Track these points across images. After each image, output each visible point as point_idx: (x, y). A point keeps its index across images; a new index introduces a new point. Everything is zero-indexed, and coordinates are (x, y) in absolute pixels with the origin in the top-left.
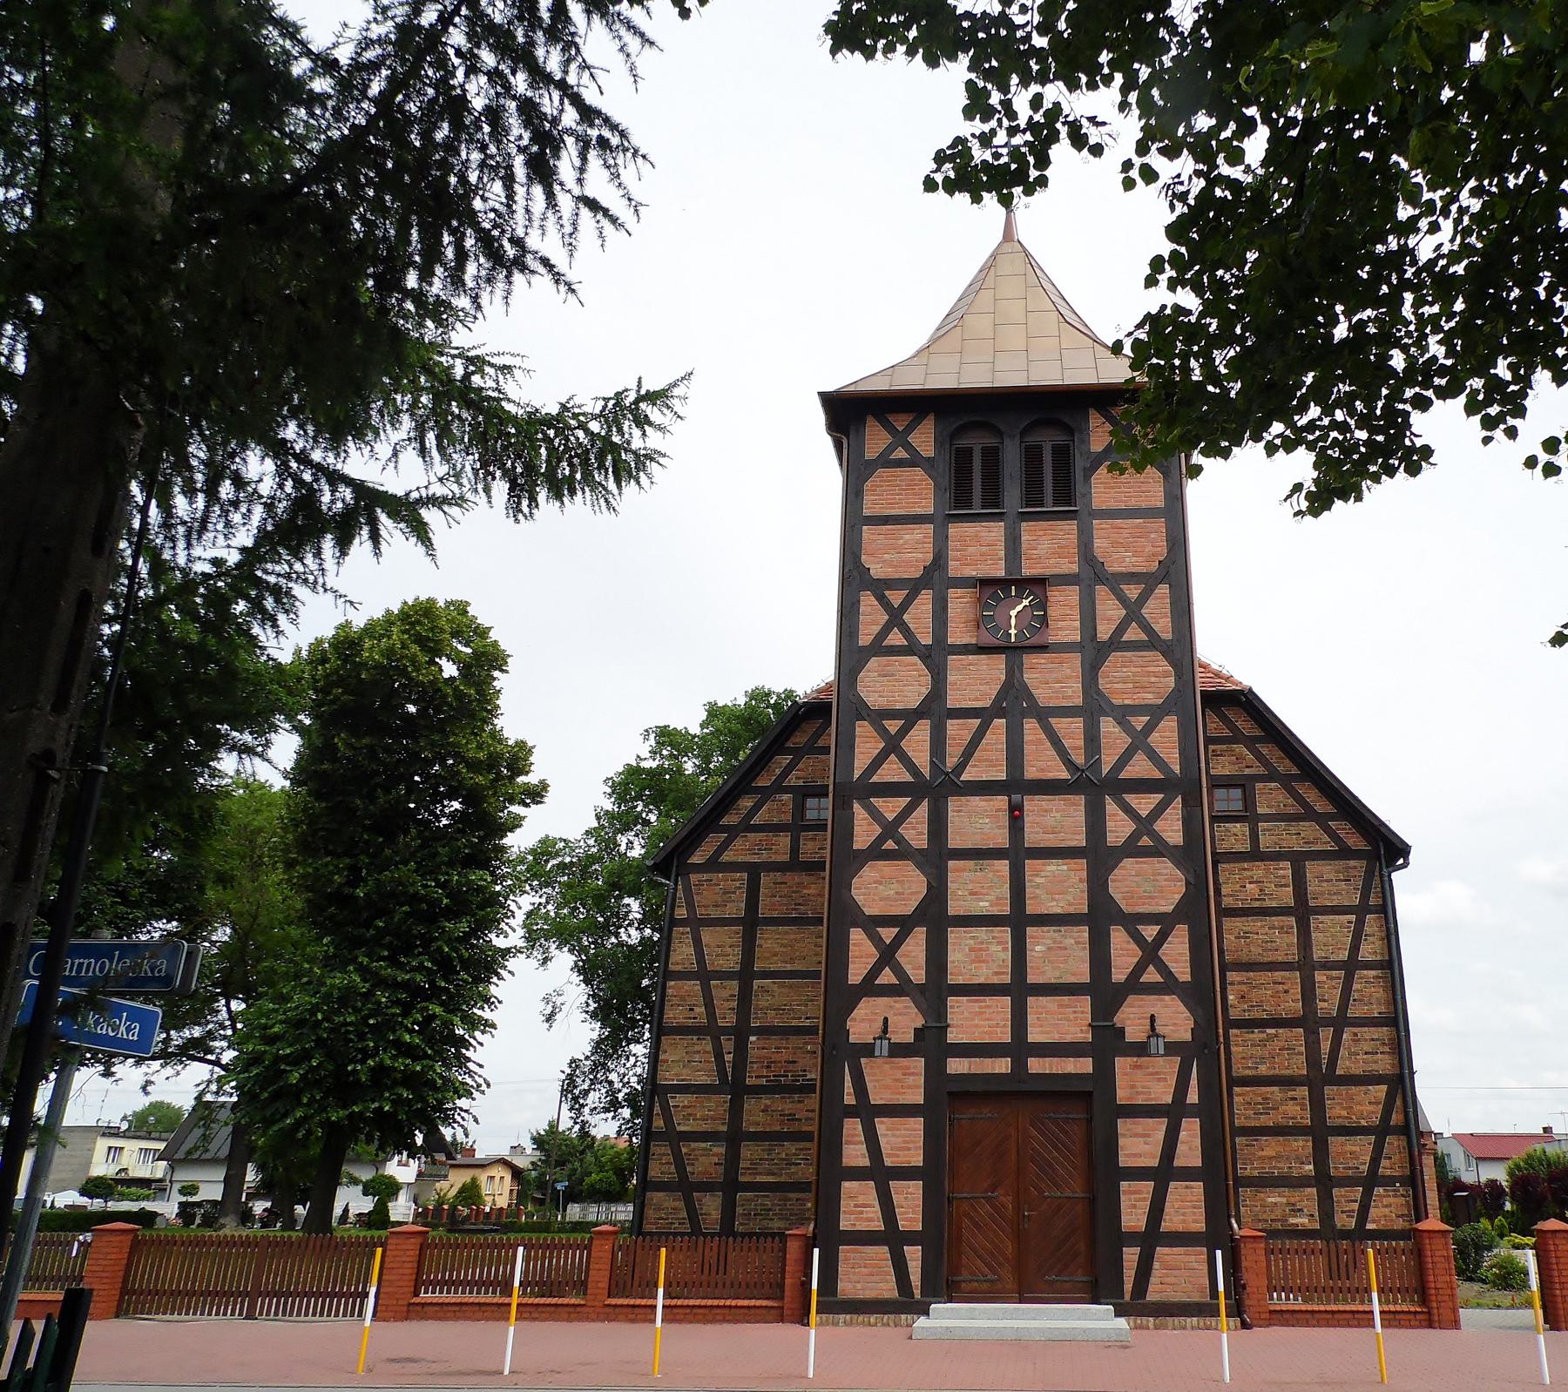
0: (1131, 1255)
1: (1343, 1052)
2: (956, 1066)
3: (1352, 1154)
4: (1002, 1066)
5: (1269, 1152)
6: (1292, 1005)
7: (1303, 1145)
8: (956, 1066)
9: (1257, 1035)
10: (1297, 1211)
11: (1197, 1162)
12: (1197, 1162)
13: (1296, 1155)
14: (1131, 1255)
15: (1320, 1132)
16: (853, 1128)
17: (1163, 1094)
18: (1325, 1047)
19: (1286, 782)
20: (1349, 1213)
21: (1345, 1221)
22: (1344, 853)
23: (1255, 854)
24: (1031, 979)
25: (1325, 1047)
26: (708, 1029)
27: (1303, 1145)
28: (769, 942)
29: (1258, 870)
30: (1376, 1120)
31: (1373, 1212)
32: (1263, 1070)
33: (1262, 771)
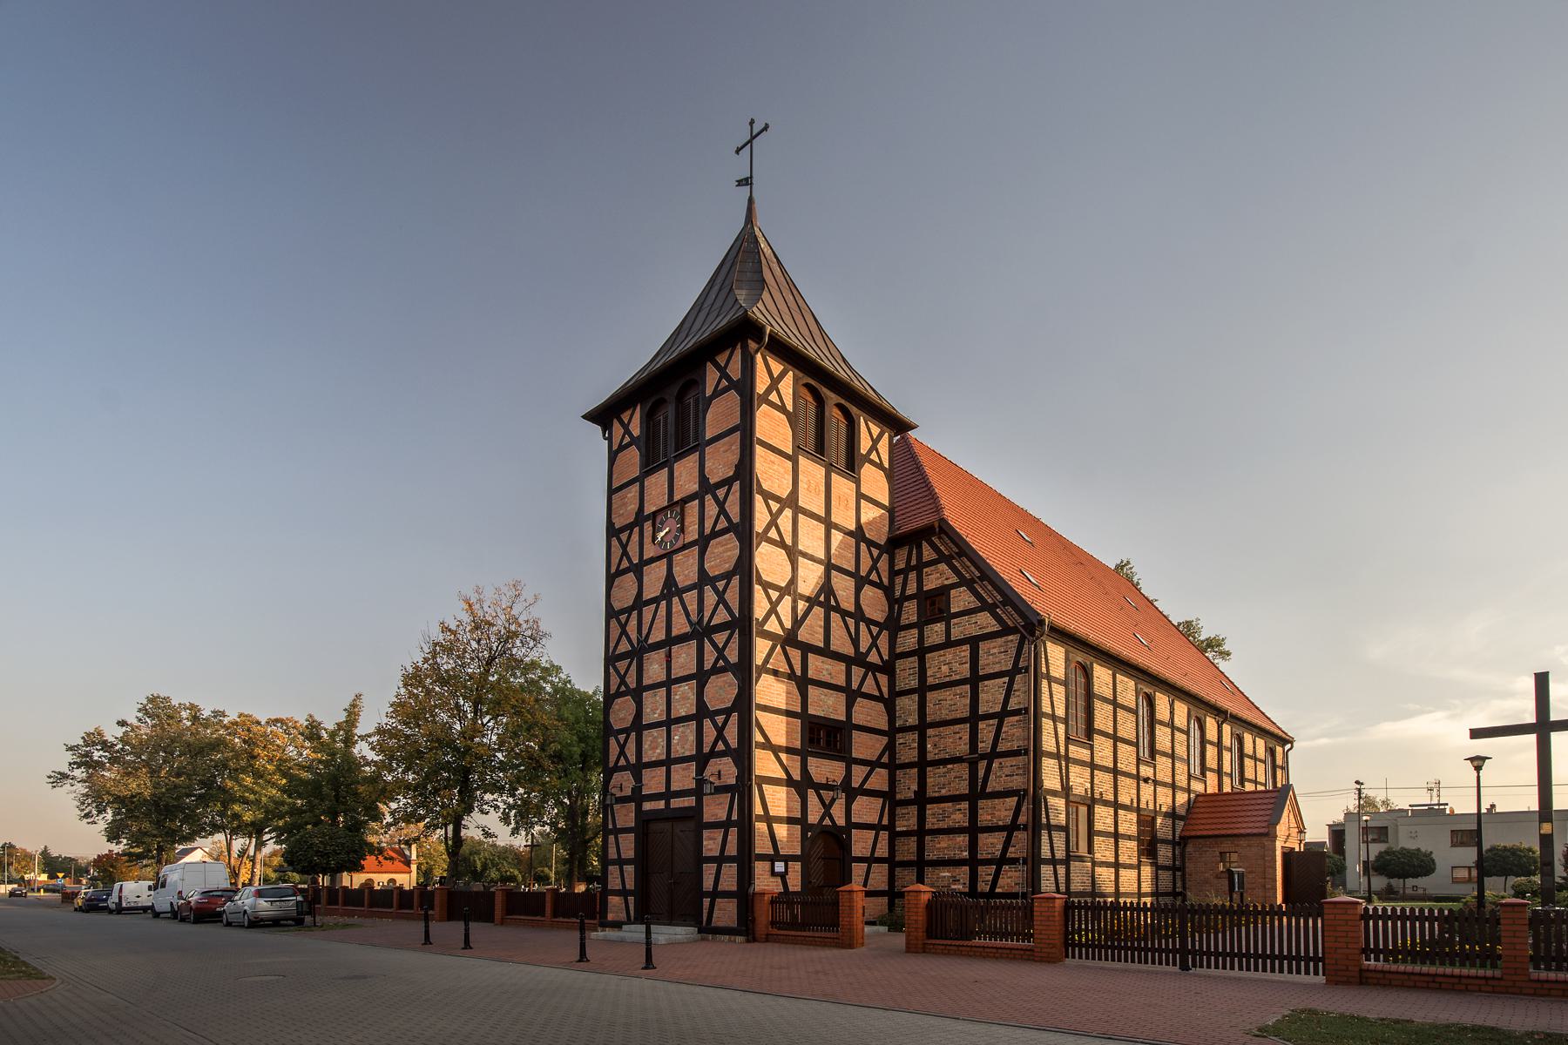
0: (706, 901)
1: (992, 777)
2: (647, 806)
3: (991, 844)
4: (661, 804)
5: (943, 845)
6: (963, 748)
7: (963, 840)
8: (647, 806)
9: (942, 770)
10: (956, 881)
11: (734, 853)
12: (734, 853)
13: (957, 846)
14: (706, 901)
15: (973, 830)
16: (630, 885)
17: (873, 819)
18: (981, 773)
19: (969, 584)
20: (986, 882)
21: (983, 887)
22: (1006, 631)
23: (949, 644)
24: (1553, 717)
25: (981, 773)
26: (617, 832)
27: (963, 840)
28: (962, 706)
29: (949, 654)
30: (1008, 821)
31: (1001, 882)
32: (944, 792)
33: (955, 579)
